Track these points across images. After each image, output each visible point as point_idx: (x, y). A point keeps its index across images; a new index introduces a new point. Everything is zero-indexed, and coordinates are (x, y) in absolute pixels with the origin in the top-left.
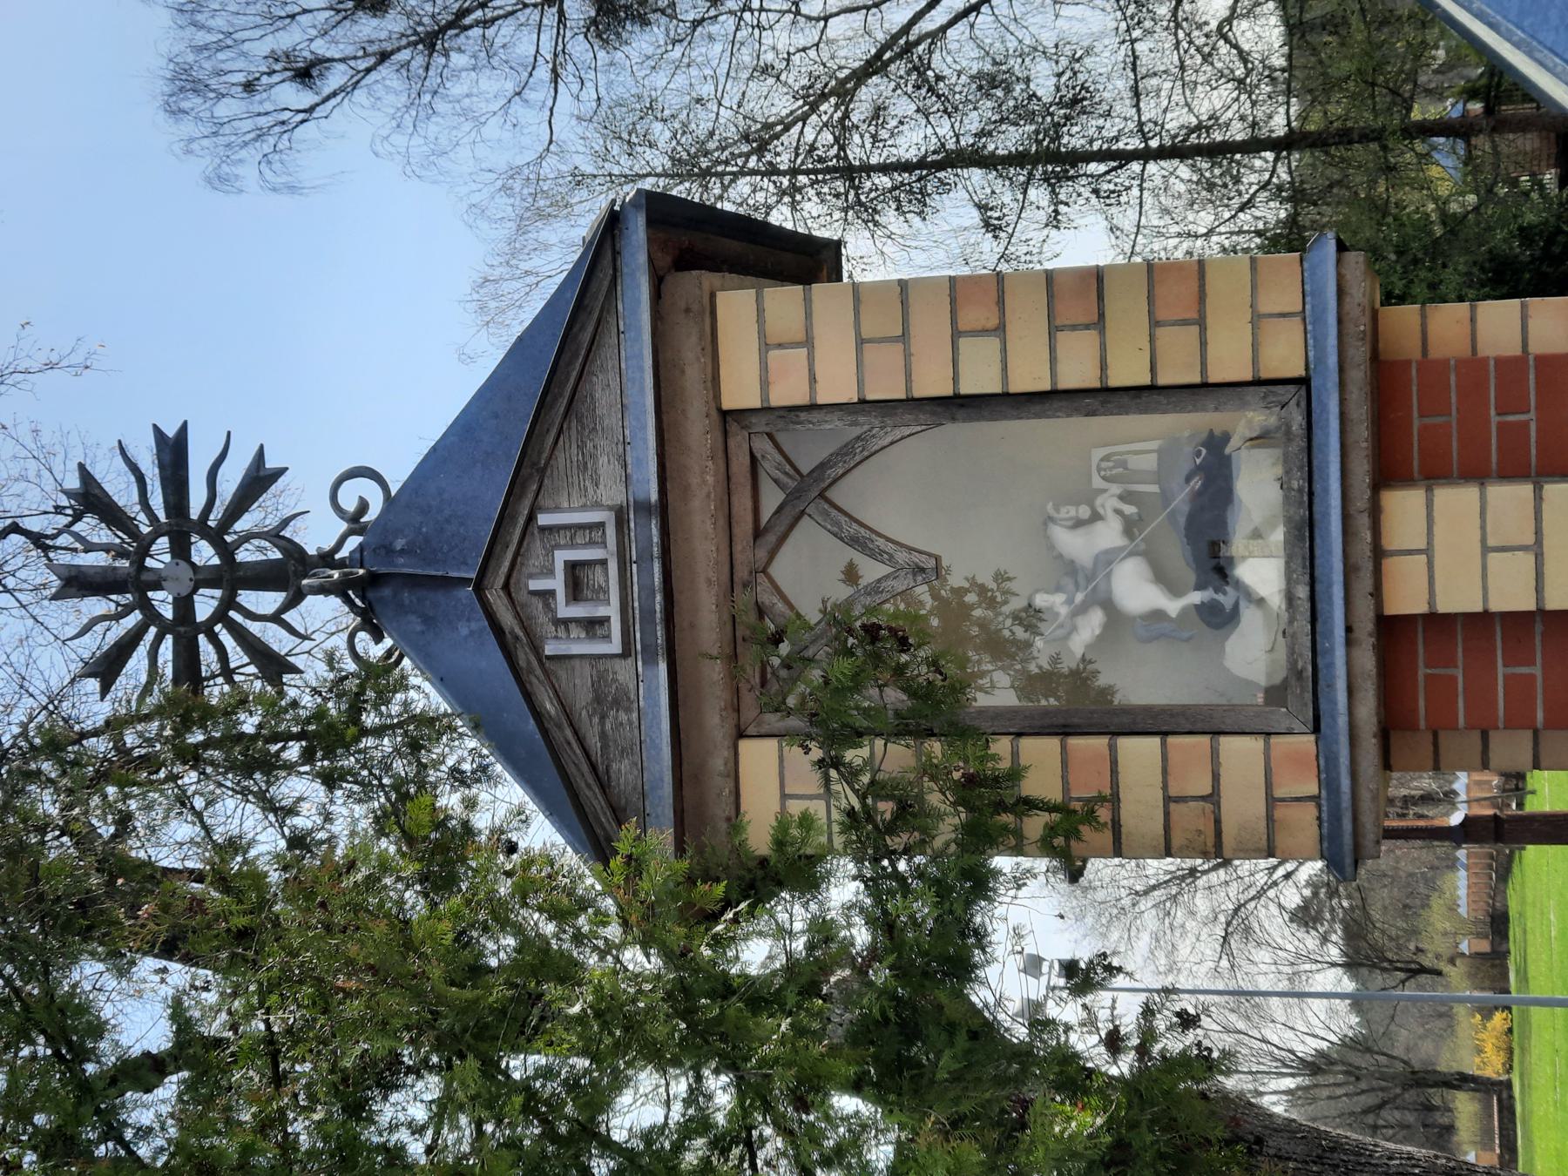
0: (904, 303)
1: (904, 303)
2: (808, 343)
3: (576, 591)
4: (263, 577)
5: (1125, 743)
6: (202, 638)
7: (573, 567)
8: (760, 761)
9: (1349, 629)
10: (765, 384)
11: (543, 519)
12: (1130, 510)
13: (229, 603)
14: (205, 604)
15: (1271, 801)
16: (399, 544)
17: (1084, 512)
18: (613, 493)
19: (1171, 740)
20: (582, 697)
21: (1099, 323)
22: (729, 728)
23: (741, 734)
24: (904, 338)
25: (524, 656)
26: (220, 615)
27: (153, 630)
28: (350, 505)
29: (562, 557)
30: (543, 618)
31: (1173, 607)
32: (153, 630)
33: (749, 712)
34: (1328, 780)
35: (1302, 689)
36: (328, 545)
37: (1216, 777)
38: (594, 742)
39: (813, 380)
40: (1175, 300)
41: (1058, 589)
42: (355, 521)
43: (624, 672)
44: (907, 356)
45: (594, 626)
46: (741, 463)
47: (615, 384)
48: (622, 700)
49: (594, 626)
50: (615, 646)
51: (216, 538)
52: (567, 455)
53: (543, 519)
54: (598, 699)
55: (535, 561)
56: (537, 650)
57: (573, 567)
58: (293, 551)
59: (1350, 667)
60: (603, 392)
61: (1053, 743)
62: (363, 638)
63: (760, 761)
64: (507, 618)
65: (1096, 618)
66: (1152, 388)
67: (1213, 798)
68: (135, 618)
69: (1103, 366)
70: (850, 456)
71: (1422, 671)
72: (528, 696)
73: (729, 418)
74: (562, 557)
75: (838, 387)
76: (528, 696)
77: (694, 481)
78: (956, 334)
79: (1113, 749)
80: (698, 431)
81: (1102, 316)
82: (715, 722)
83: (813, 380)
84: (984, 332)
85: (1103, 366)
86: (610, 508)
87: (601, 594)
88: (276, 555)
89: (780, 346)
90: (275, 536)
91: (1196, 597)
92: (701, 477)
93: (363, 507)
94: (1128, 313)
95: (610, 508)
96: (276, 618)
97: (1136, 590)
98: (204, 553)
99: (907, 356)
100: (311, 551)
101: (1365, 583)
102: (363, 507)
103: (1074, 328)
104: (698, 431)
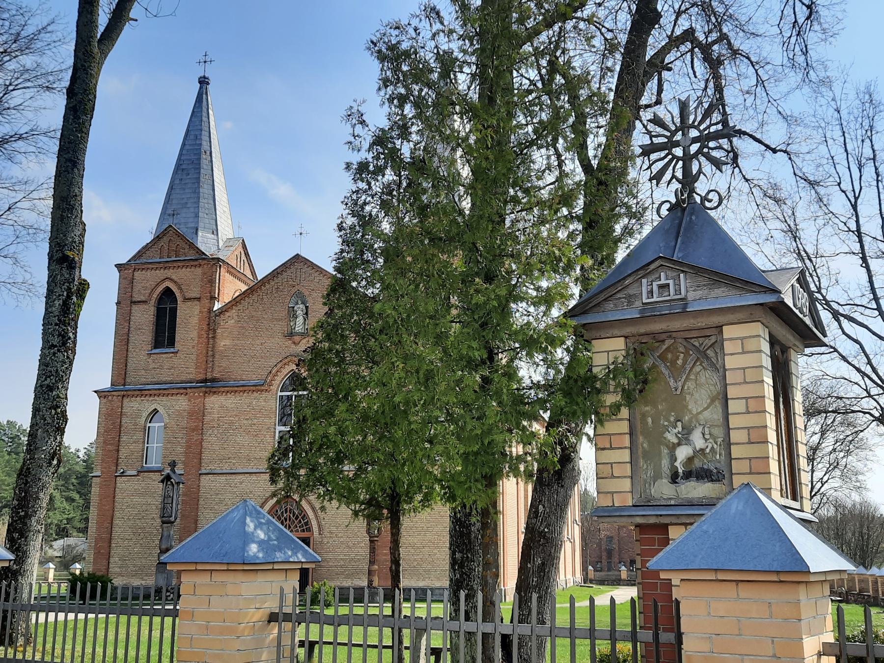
0: (757, 382)
1: (757, 382)
2: (744, 352)
3: (661, 287)
4: (686, 169)
5: (628, 451)
6: (667, 152)
7: (668, 285)
8: (619, 344)
9: (661, 515)
10: (731, 339)
11: (682, 275)
12: (708, 450)
13: (678, 159)
14: (694, 133)
15: (612, 493)
16: (693, 218)
17: (707, 437)
18: (691, 296)
19: (629, 465)
20: (632, 291)
21: (750, 442)
22: (627, 335)
23: (626, 337)
24: (746, 382)
25: (641, 273)
26: (674, 157)
27: (668, 134)
28: (710, 197)
29: (671, 282)
30: (653, 277)
31: (677, 464)
32: (668, 134)
33: (633, 340)
34: (620, 508)
35: (646, 503)
36: (698, 191)
37: (618, 477)
38: (619, 295)
39: (732, 354)
40: (757, 466)
41: (683, 428)
42: (705, 199)
43: (638, 304)
44: (739, 384)
45: (651, 293)
46: (707, 332)
47: (724, 294)
48: (630, 303)
49: (651, 293)
50: (644, 301)
51: (699, 152)
52: (702, 281)
53: (682, 275)
54: (630, 296)
55: (670, 273)
56: (643, 277)
57: (668, 285)
58: (696, 178)
59: (650, 516)
60: (720, 291)
61: (627, 430)
62: (667, 206)
63: (619, 344)
64: (652, 267)
65: (675, 441)
66: (731, 459)
67: (613, 477)
68: (673, 128)
69: (737, 444)
70: (713, 366)
71: (657, 536)
72: (630, 275)
73: (720, 328)
74: (671, 282)
75: (730, 362)
76: (630, 275)
77: (699, 320)
78: (747, 398)
79: (625, 448)
80: (715, 320)
81: (753, 443)
82: (629, 330)
83: (732, 354)
84: (747, 407)
85: (737, 444)
86: (686, 296)
87: (660, 295)
88: (694, 172)
89: (742, 344)
90: (700, 171)
91: (680, 471)
92: (702, 322)
93: (710, 201)
94: (754, 451)
95: (686, 296)
96: (673, 177)
97: (683, 453)
98: (694, 148)
99: (739, 384)
100: (696, 185)
101: (674, 520)
102: (710, 201)
103: (749, 434)
104: (715, 320)
